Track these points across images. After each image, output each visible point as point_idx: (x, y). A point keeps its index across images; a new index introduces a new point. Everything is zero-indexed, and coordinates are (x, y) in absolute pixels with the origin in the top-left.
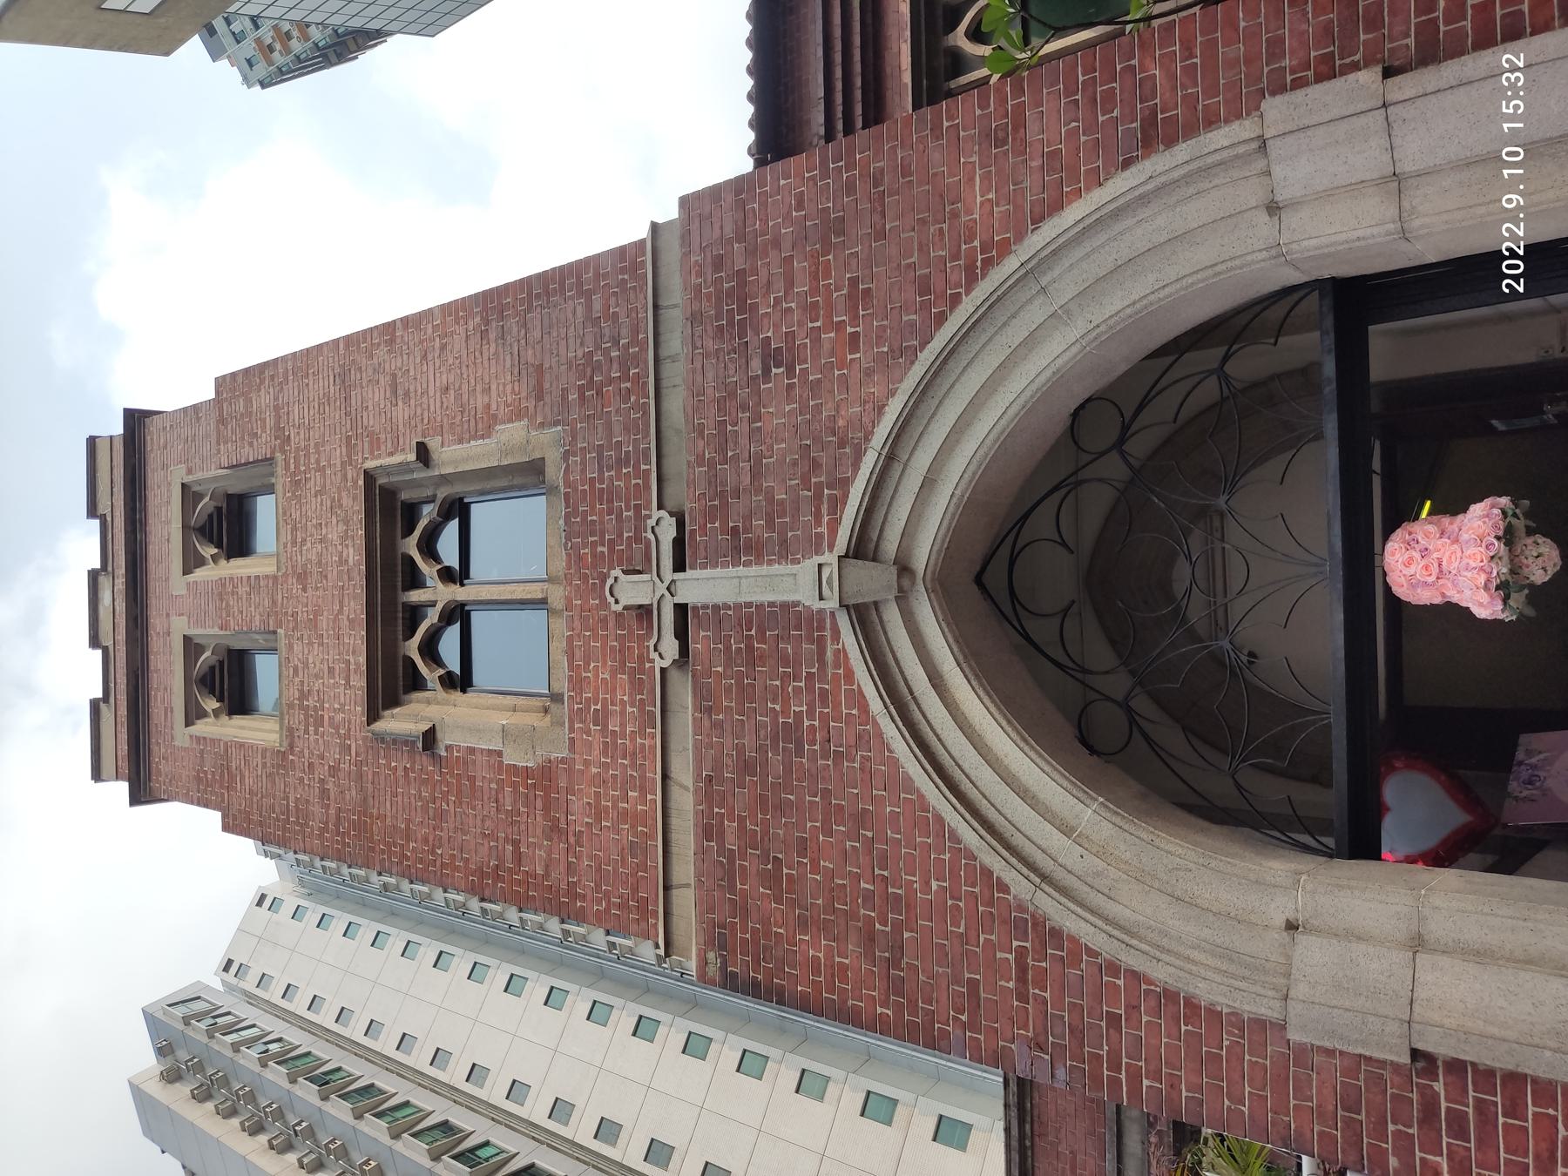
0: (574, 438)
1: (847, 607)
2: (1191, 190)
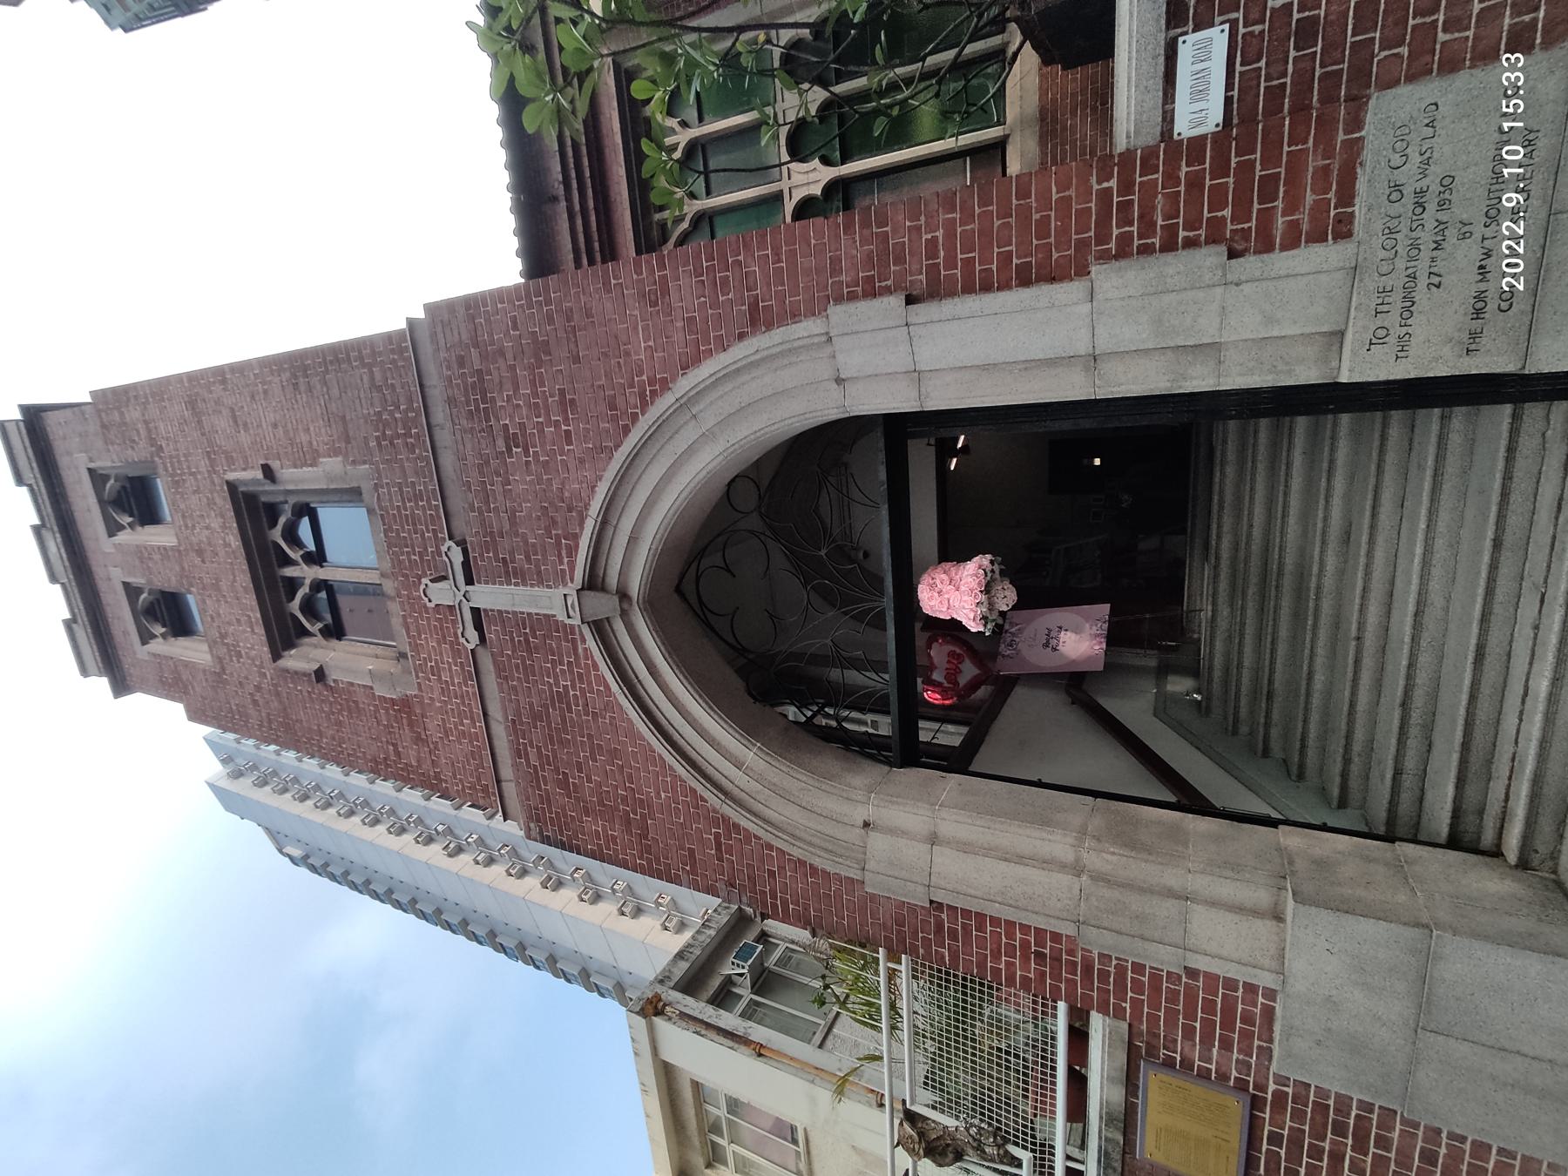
1: (588, 623)
2: (786, 362)
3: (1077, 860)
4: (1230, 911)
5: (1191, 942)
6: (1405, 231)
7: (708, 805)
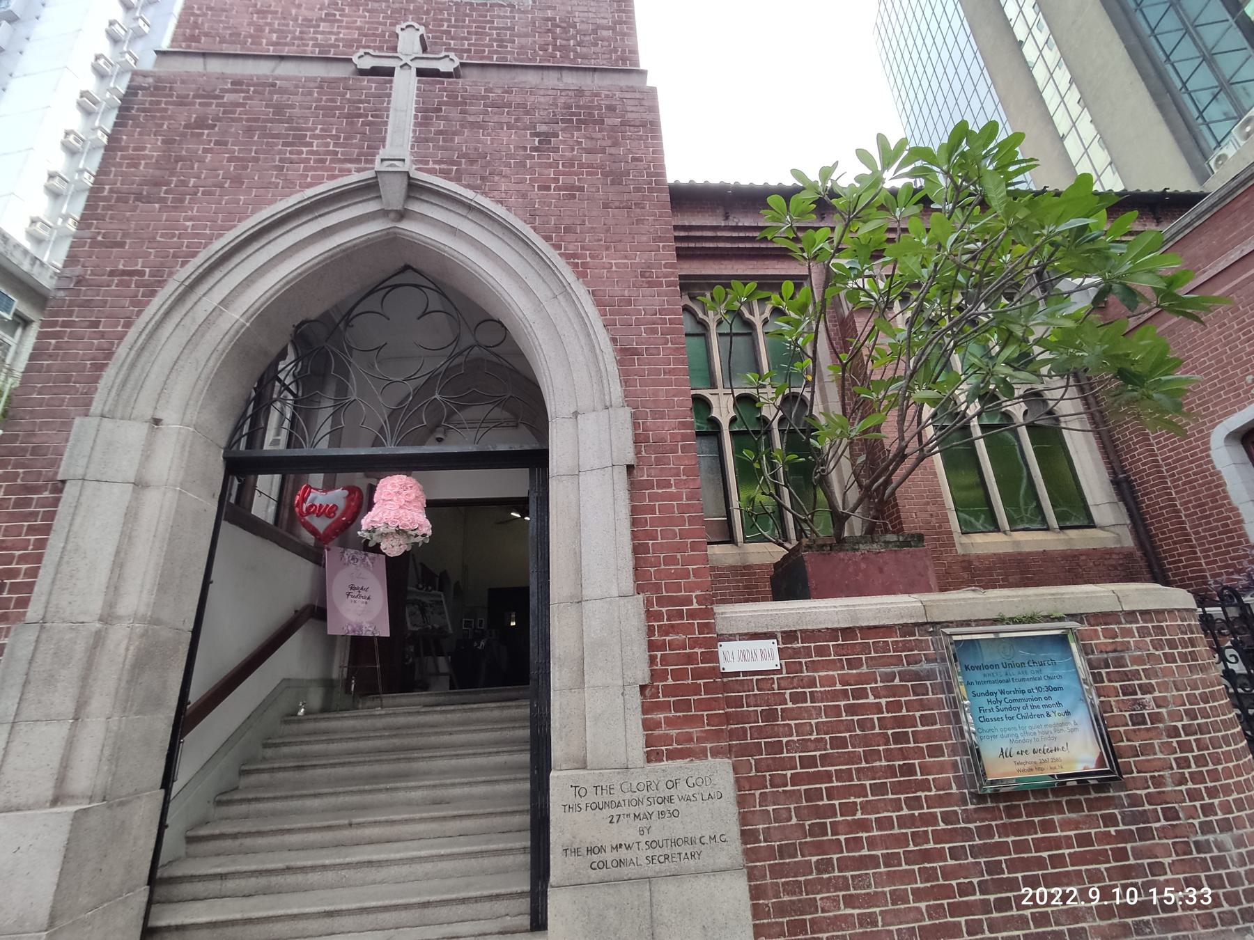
0: (523, 12)
1: (376, 177)
2: (593, 373)
3: (120, 618)
4: (62, 759)
5: (22, 727)
6: (648, 795)
7: (178, 268)
